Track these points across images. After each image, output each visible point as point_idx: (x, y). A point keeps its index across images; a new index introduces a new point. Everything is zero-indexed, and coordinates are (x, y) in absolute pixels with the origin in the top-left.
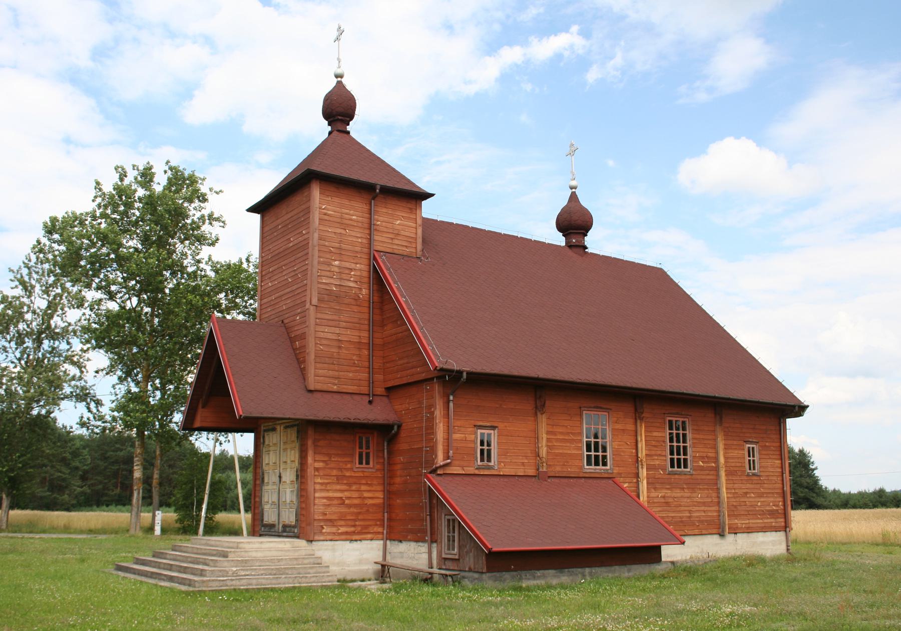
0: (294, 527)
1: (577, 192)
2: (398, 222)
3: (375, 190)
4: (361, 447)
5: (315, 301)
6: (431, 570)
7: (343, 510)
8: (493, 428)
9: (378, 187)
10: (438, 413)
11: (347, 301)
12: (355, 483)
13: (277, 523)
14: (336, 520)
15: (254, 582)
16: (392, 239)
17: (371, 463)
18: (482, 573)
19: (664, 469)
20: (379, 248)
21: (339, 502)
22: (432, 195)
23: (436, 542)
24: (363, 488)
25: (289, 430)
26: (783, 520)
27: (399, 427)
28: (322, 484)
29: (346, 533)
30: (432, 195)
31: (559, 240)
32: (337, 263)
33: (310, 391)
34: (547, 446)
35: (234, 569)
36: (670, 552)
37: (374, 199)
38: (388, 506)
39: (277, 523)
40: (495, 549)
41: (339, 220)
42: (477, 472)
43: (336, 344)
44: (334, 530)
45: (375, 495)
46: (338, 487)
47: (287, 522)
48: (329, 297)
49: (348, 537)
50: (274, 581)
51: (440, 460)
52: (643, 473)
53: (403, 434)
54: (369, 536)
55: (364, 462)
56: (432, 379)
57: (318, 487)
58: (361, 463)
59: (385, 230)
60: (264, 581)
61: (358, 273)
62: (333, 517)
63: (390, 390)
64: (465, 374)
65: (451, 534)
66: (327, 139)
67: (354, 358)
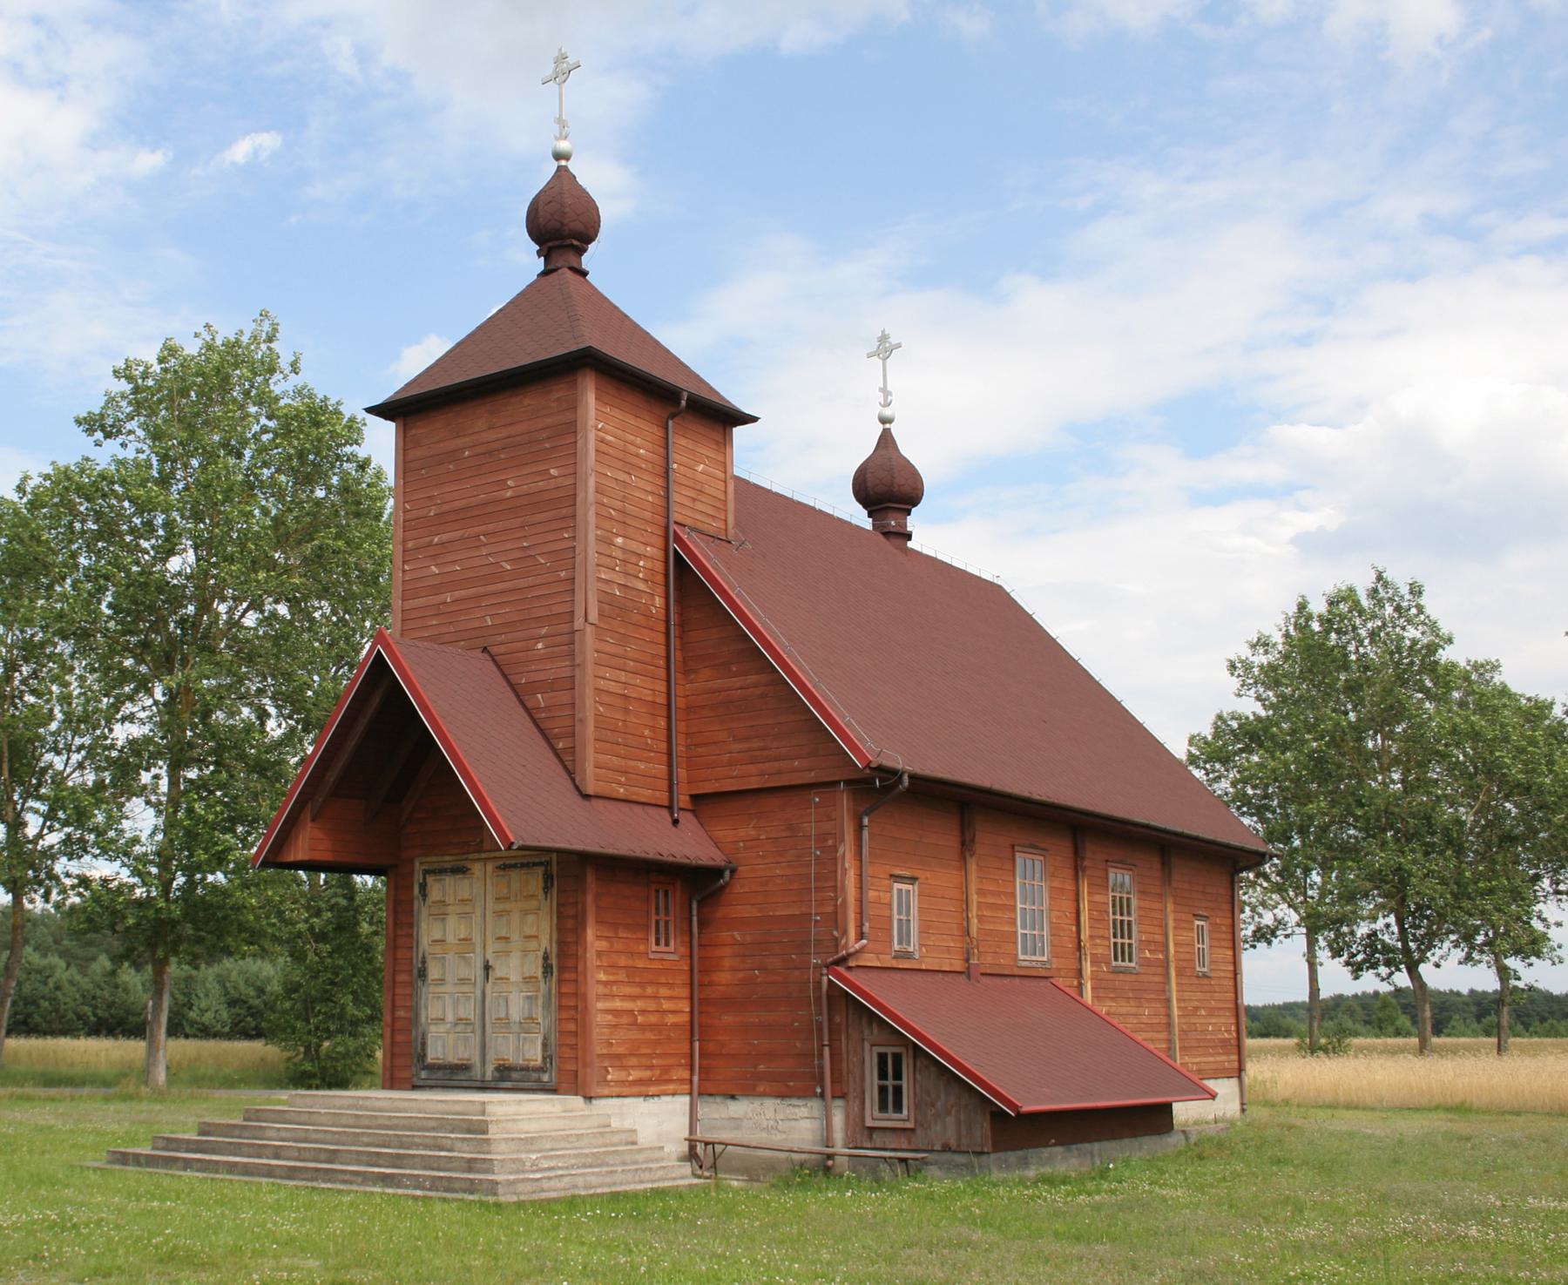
0: (542, 1070)
1: (893, 428)
2: (701, 467)
4: (657, 913)
6: (830, 1150)
7: (635, 1035)
8: (912, 880)
9: (685, 395)
10: (847, 849)
11: (636, 618)
12: (651, 983)
13: (476, 1059)
14: (625, 1055)
15: (580, 1181)
16: (694, 500)
17: (672, 943)
18: (982, 1153)
19: (1108, 963)
22: (754, 419)
23: (843, 1096)
24: (664, 991)
25: (515, 875)
27: (733, 871)
28: (605, 983)
30: (754, 419)
31: (859, 517)
32: (619, 540)
33: (587, 797)
35: (534, 1157)
36: (1183, 1111)
37: (672, 416)
38: (697, 1028)
39: (476, 1059)
40: (1026, 1108)
41: (620, 455)
42: (895, 964)
44: (621, 1075)
45: (676, 1009)
46: (628, 990)
47: (511, 1058)
48: (614, 608)
49: (643, 1089)
50: (608, 1180)
52: (1088, 968)
53: (739, 888)
54: (671, 1087)
55: (662, 941)
56: (835, 783)
58: (657, 944)
60: (593, 1180)
61: (649, 565)
62: (621, 1050)
63: (701, 802)
65: (890, 1083)
67: (647, 732)
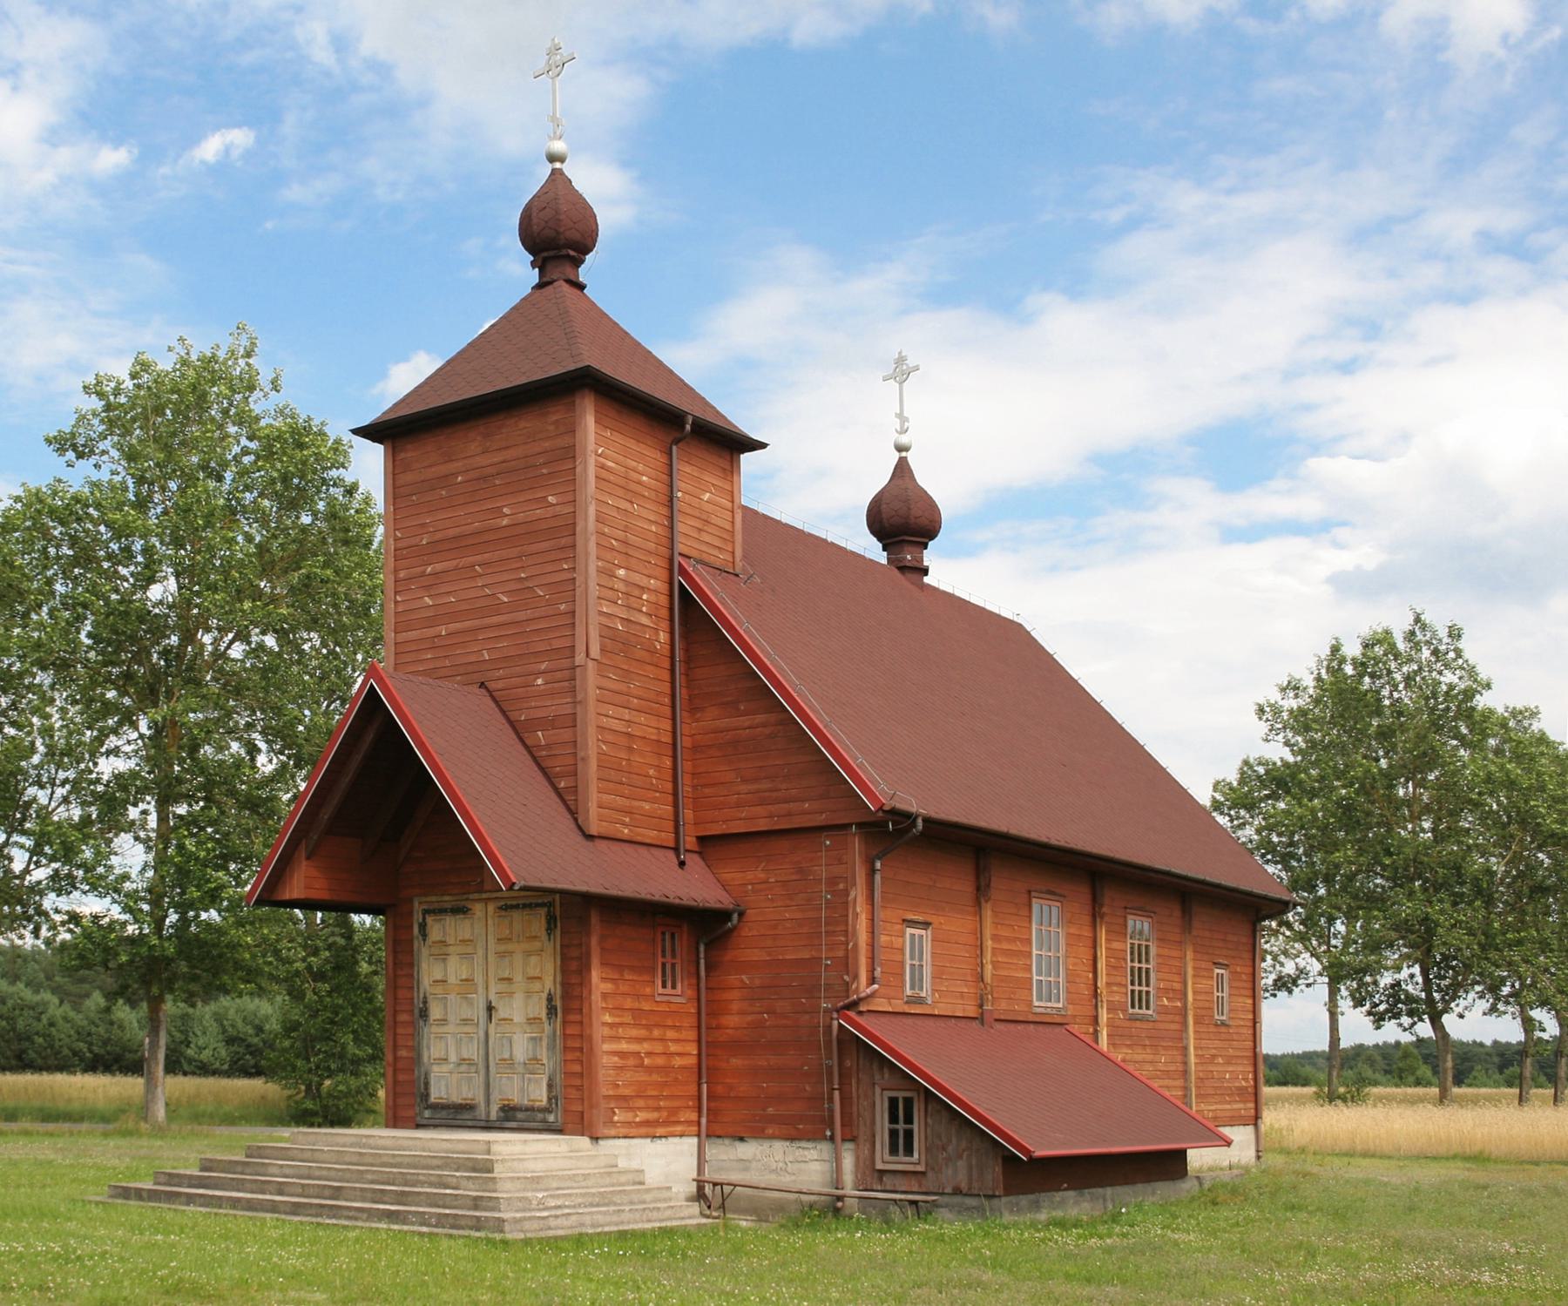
0: (547, 1110)
2: (707, 496)
3: (683, 427)
5: (595, 651)
6: (839, 1192)
8: (926, 925)
10: (858, 894)
12: (657, 1026)
13: (480, 1099)
15: (587, 1220)
16: (700, 530)
17: (679, 985)
19: (1125, 1011)
20: (685, 551)
21: (637, 1062)
22: (763, 446)
23: (853, 1139)
24: (670, 1034)
26: (1252, 1105)
27: (741, 914)
28: (612, 1026)
29: (647, 1123)
31: (874, 550)
32: (622, 572)
33: (590, 837)
34: (992, 962)
36: (1197, 1158)
37: (677, 442)
38: (705, 1070)
39: (480, 1099)
40: (1039, 1153)
41: (622, 482)
42: (907, 1009)
43: (623, 741)
44: (628, 1116)
45: (683, 1050)
46: (634, 1032)
47: (516, 1098)
49: (651, 1130)
51: (863, 988)
53: (748, 931)
54: (679, 1128)
55: (669, 984)
57: (606, 1031)
58: (664, 986)
59: (689, 511)
61: (653, 598)
62: (627, 1092)
63: (708, 844)
64: (920, 822)
65: (901, 1126)
66: (530, 295)
67: (651, 772)
